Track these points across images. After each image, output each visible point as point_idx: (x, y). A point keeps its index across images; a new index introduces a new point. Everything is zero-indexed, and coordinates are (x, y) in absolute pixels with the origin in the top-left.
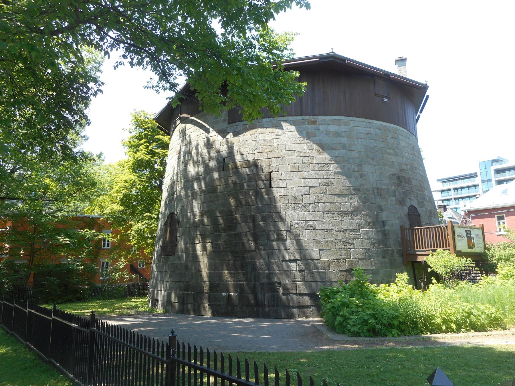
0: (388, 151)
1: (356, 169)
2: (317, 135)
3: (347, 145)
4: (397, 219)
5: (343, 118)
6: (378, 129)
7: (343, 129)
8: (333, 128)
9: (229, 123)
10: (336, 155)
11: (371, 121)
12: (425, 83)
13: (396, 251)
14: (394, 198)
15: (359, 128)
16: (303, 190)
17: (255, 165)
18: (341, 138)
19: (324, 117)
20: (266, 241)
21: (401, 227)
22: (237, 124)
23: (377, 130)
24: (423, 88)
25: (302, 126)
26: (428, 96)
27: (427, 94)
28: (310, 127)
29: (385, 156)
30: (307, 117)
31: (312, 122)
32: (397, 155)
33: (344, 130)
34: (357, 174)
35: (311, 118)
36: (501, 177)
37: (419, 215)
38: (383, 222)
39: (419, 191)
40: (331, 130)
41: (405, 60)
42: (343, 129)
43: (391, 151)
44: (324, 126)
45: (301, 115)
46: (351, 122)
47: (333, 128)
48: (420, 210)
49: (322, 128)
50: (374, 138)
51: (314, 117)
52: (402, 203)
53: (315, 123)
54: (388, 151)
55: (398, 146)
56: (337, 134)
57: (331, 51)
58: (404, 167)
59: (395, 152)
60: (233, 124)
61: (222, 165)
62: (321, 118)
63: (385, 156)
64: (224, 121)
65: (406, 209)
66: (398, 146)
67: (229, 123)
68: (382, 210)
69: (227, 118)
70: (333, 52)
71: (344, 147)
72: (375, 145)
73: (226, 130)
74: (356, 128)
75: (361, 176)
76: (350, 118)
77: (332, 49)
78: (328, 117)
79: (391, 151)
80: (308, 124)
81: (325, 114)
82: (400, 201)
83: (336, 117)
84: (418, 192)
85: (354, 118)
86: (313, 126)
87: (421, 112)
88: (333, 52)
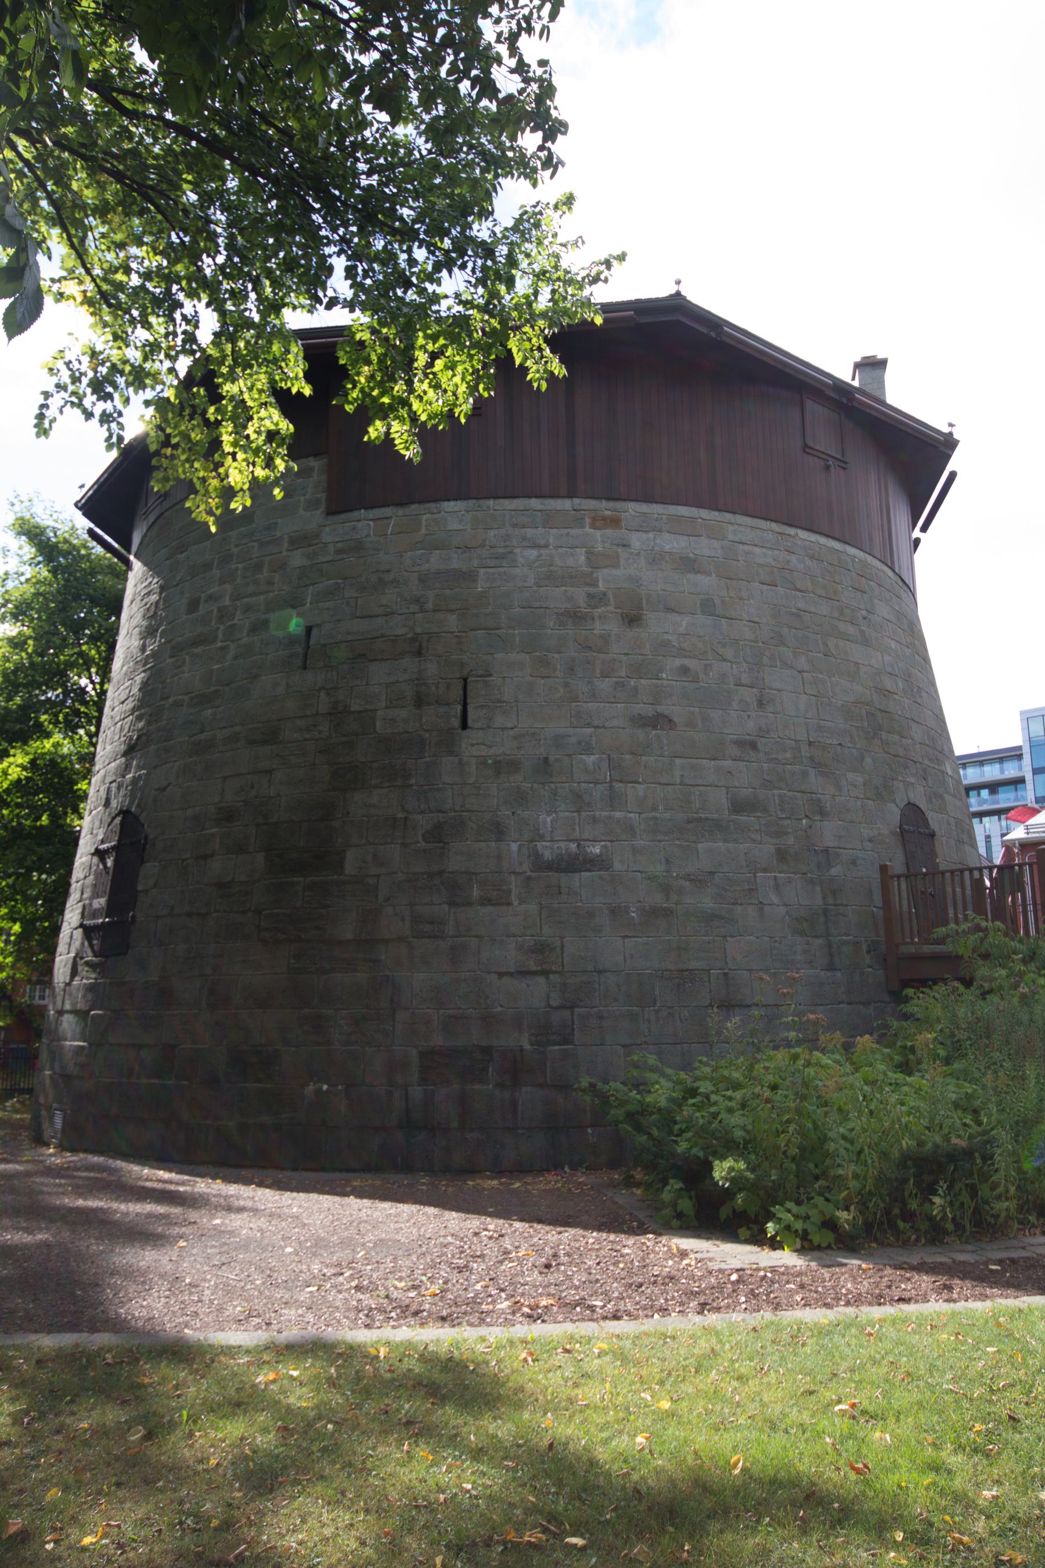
0: (842, 626)
1: (745, 679)
2: (622, 562)
3: (717, 602)
4: (868, 845)
5: (704, 513)
6: (812, 557)
7: (705, 548)
8: (673, 544)
9: (330, 513)
10: (682, 630)
11: (792, 531)
12: (946, 430)
13: (864, 947)
14: (859, 779)
15: (757, 550)
16: (573, 740)
17: (538, 112)
18: (700, 577)
19: (644, 507)
20: (446, 907)
21: (884, 869)
22: (355, 514)
23: (808, 562)
24: (946, 445)
25: (573, 532)
26: (953, 476)
27: (949, 468)
28: (598, 534)
29: (832, 642)
30: (590, 504)
31: (604, 519)
32: (866, 642)
33: (706, 552)
34: (748, 695)
35: (605, 507)
36: (1011, 771)
37: (932, 835)
38: (826, 850)
39: (931, 760)
40: (667, 548)
41: (882, 364)
42: (705, 548)
43: (851, 630)
44: (644, 535)
45: (571, 495)
46: (731, 528)
47: (673, 544)
48: (934, 820)
49: (637, 540)
50: (799, 585)
51: (612, 504)
52: (882, 792)
53: (615, 522)
54: (842, 626)
55: (870, 616)
56: (689, 564)
57: (673, 292)
58: (888, 683)
59: (862, 632)
60: (343, 516)
61: (299, 649)
62: (633, 509)
63: (832, 642)
64: (312, 505)
65: (893, 813)
66: (870, 616)
67: (330, 513)
68: (822, 813)
69: (323, 496)
70: (678, 294)
71: (708, 606)
72: (801, 605)
73: (317, 536)
74: (746, 547)
75: (760, 704)
76: (728, 516)
77: (678, 282)
78: (656, 509)
79: (851, 630)
80: (593, 526)
81: (649, 499)
82: (877, 788)
83: (683, 511)
84: (926, 762)
85: (740, 519)
86: (609, 532)
87: (924, 529)
88: (678, 294)
